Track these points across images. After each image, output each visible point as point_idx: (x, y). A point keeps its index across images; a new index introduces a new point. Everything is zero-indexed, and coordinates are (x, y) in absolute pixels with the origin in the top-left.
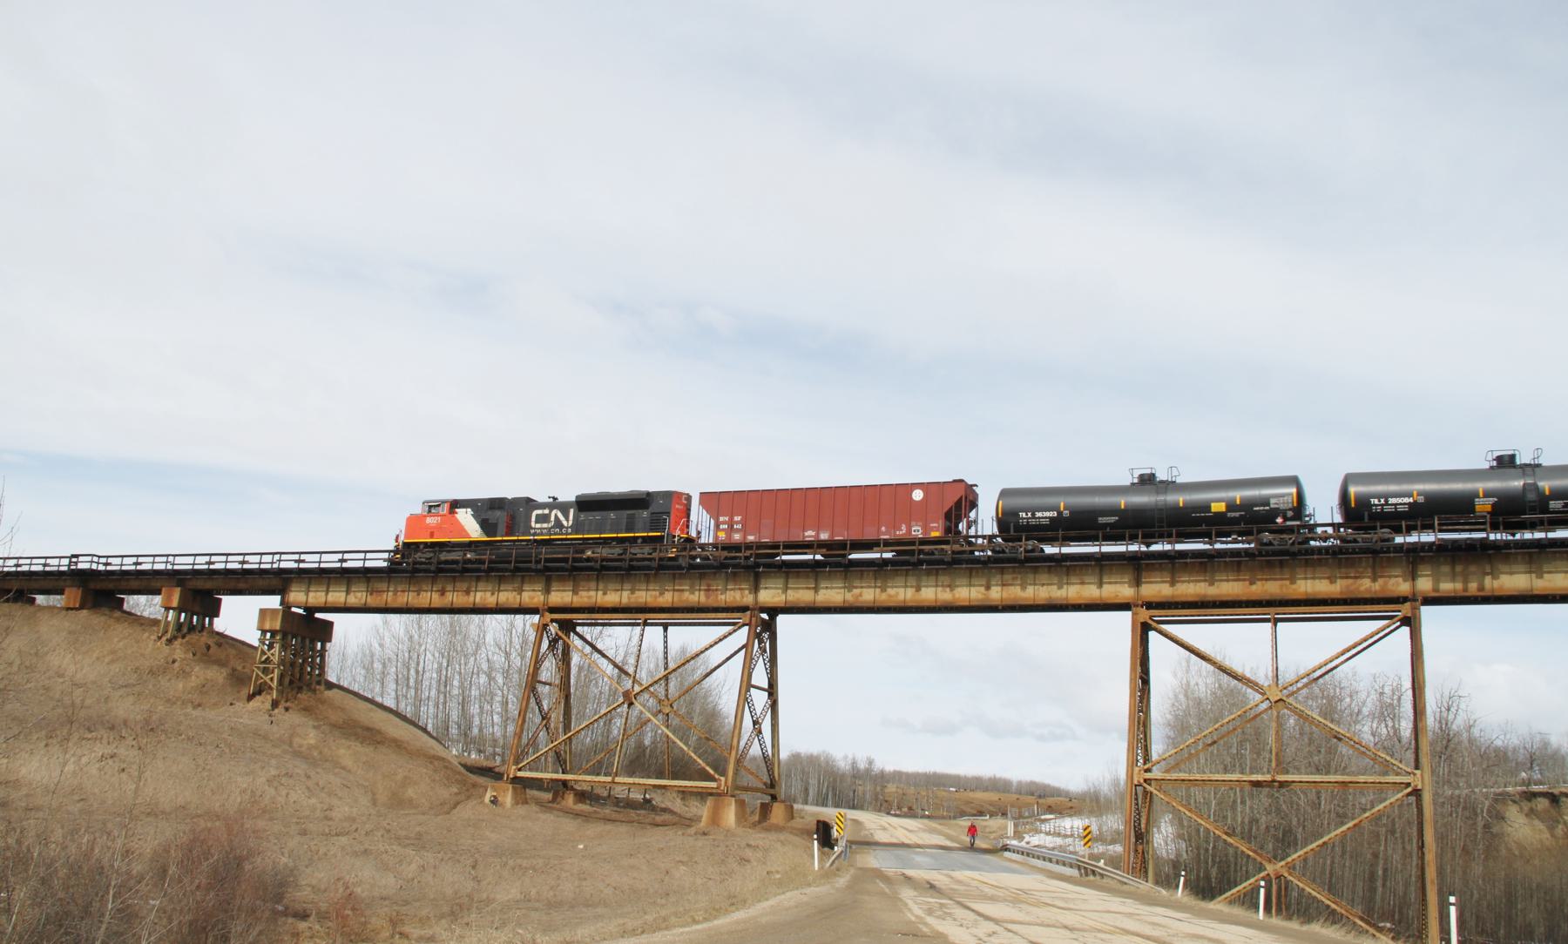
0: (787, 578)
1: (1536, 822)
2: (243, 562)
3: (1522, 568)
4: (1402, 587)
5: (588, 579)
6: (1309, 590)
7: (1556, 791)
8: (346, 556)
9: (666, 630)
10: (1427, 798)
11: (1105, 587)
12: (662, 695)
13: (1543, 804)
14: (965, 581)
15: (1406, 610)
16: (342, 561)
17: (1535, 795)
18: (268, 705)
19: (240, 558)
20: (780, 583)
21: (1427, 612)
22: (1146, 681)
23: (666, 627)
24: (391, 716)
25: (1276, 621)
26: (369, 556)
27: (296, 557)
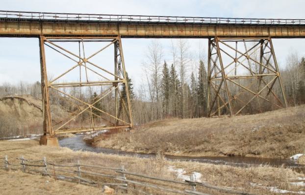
0: (30, 26)
1: (7, 105)
2: (258, 22)
3: (143, 29)
4: (115, 32)
5: (259, 29)
6: (23, 31)
7: (13, 97)
8: (294, 21)
9: (237, 43)
10: (126, 84)
11: (67, 30)
12: (238, 57)
13: (9, 100)
14: (79, 28)
15: (269, 38)
16: (229, 21)
17: (7, 98)
18: (167, 63)
19: (278, 21)
20: (125, 28)
21: (272, 39)
22: (41, 58)
23: (237, 42)
24: (63, 76)
25: (79, 41)
26: (301, 21)
27: (257, 20)
